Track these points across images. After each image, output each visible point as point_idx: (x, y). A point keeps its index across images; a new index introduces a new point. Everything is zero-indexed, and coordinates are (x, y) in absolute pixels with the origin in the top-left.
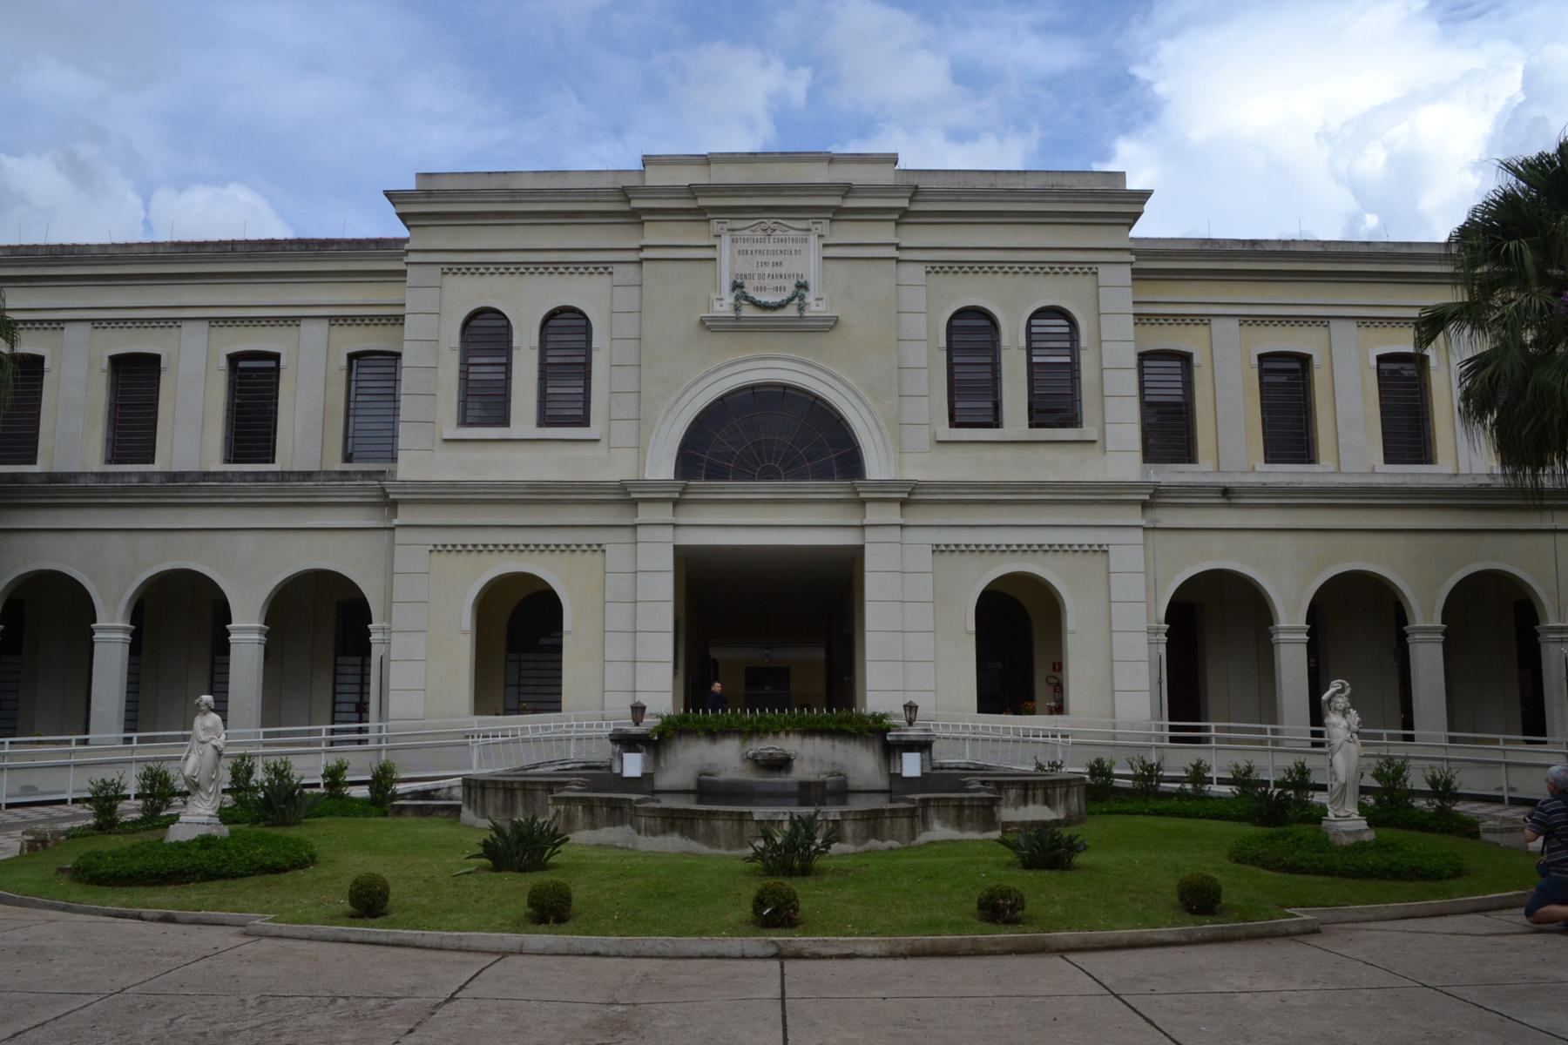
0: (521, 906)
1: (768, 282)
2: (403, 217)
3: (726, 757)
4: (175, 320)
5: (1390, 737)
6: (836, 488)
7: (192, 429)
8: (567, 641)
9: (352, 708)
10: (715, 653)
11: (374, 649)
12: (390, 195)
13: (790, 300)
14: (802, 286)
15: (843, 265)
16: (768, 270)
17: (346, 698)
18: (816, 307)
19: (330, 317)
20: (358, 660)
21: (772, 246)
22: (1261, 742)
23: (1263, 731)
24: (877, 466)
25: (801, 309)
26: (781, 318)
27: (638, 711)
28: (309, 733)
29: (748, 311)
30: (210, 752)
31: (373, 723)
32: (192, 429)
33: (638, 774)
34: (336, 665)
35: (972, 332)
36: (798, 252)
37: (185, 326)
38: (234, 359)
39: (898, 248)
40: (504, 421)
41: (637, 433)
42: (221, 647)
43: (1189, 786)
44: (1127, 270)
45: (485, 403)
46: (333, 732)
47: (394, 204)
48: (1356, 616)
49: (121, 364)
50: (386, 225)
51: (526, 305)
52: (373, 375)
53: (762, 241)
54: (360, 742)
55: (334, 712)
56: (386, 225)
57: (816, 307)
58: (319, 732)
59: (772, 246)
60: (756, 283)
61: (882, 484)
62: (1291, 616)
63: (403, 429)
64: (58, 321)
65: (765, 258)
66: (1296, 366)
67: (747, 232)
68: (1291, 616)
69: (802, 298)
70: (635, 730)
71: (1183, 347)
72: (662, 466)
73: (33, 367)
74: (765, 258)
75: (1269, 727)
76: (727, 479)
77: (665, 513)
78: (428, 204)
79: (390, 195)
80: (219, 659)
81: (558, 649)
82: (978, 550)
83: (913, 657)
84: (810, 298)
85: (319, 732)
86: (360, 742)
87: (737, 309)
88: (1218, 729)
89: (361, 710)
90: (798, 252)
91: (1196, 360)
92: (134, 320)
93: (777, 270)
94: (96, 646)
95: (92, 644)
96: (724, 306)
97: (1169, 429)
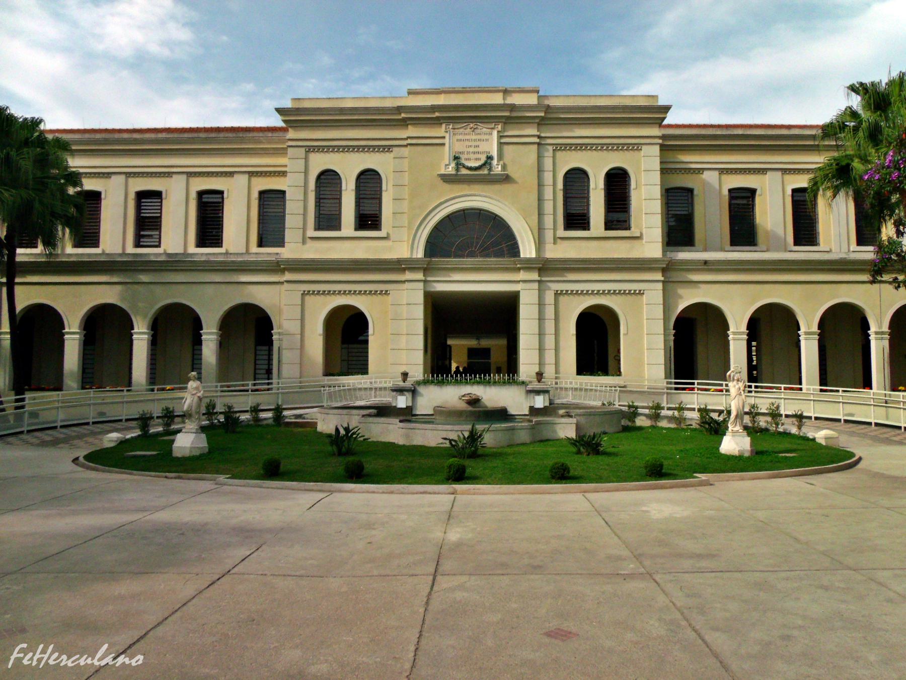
0: (341, 470)
1: (472, 156)
2: (284, 121)
3: (451, 395)
4: (169, 173)
5: (785, 389)
6: (506, 261)
7: (177, 233)
8: (371, 339)
9: (264, 371)
10: (449, 342)
11: (275, 342)
12: (278, 110)
13: (484, 164)
14: (490, 158)
15: (515, 147)
16: (472, 150)
17: (261, 367)
18: (497, 169)
19: (249, 172)
20: (266, 348)
21: (474, 137)
22: (721, 391)
23: (693, 384)
24: (528, 250)
25: (490, 170)
26: (483, 175)
27: (405, 375)
28: (243, 385)
29: (464, 171)
30: (196, 399)
31: (274, 381)
32: (177, 233)
33: (404, 406)
34: (256, 350)
35: (576, 179)
36: (487, 140)
37: (174, 176)
38: (201, 194)
39: (539, 137)
40: (338, 227)
41: (403, 235)
42: (197, 341)
43: (676, 413)
44: (657, 148)
45: (328, 220)
46: (255, 385)
47: (281, 115)
48: (772, 328)
49: (142, 196)
50: (277, 121)
51: (348, 168)
52: (271, 204)
53: (469, 134)
54: (268, 390)
55: (255, 374)
56: (277, 121)
57: (497, 169)
58: (248, 385)
59: (474, 137)
60: (466, 156)
61: (529, 260)
62: (738, 327)
63: (287, 231)
64: (109, 173)
65: (470, 143)
66: (749, 195)
67: (462, 130)
68: (738, 327)
69: (490, 164)
70: (401, 384)
71: (690, 185)
72: (420, 254)
73: (95, 197)
74: (470, 143)
75: (724, 383)
76: (449, 257)
77: (420, 276)
78: (296, 117)
79: (278, 110)
80: (196, 347)
81: (366, 342)
82: (577, 293)
83: (545, 342)
84: (495, 162)
85: (248, 385)
86: (268, 390)
87: (457, 170)
88: (698, 384)
89: (269, 372)
90: (487, 140)
91: (695, 192)
92: (147, 173)
93: (476, 150)
94: (135, 342)
95: (63, 341)
96: (451, 170)
97: (680, 230)
